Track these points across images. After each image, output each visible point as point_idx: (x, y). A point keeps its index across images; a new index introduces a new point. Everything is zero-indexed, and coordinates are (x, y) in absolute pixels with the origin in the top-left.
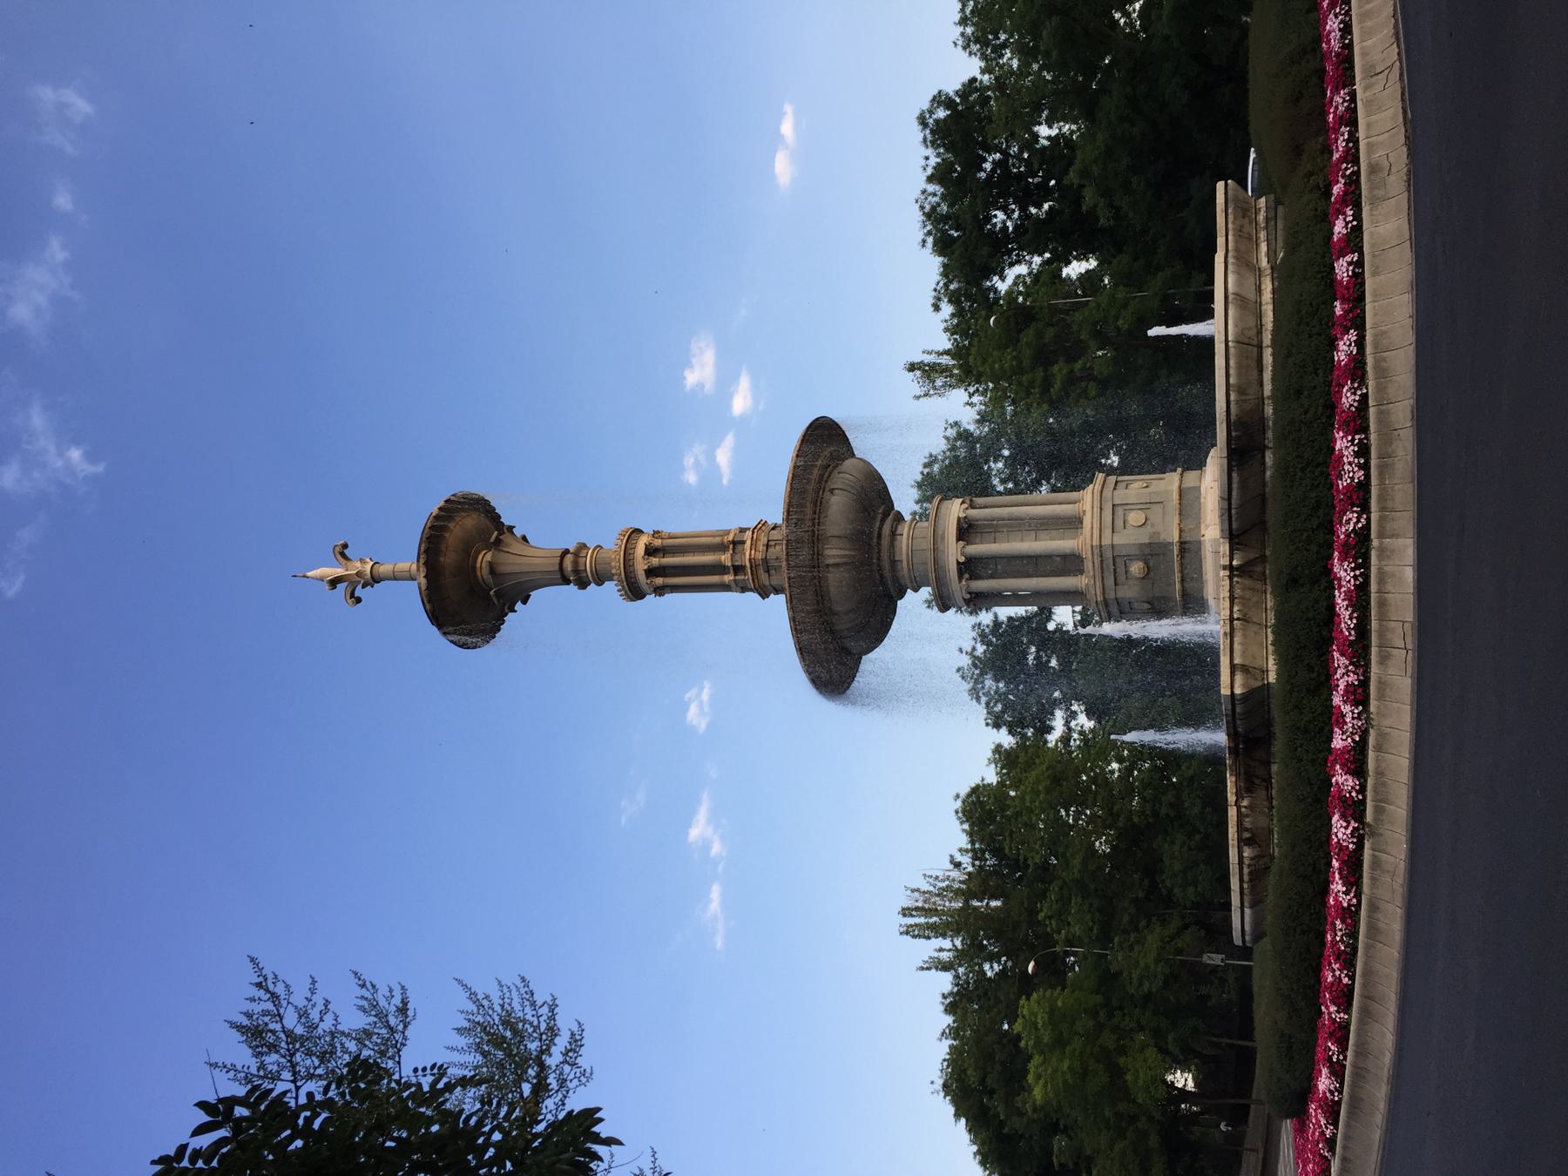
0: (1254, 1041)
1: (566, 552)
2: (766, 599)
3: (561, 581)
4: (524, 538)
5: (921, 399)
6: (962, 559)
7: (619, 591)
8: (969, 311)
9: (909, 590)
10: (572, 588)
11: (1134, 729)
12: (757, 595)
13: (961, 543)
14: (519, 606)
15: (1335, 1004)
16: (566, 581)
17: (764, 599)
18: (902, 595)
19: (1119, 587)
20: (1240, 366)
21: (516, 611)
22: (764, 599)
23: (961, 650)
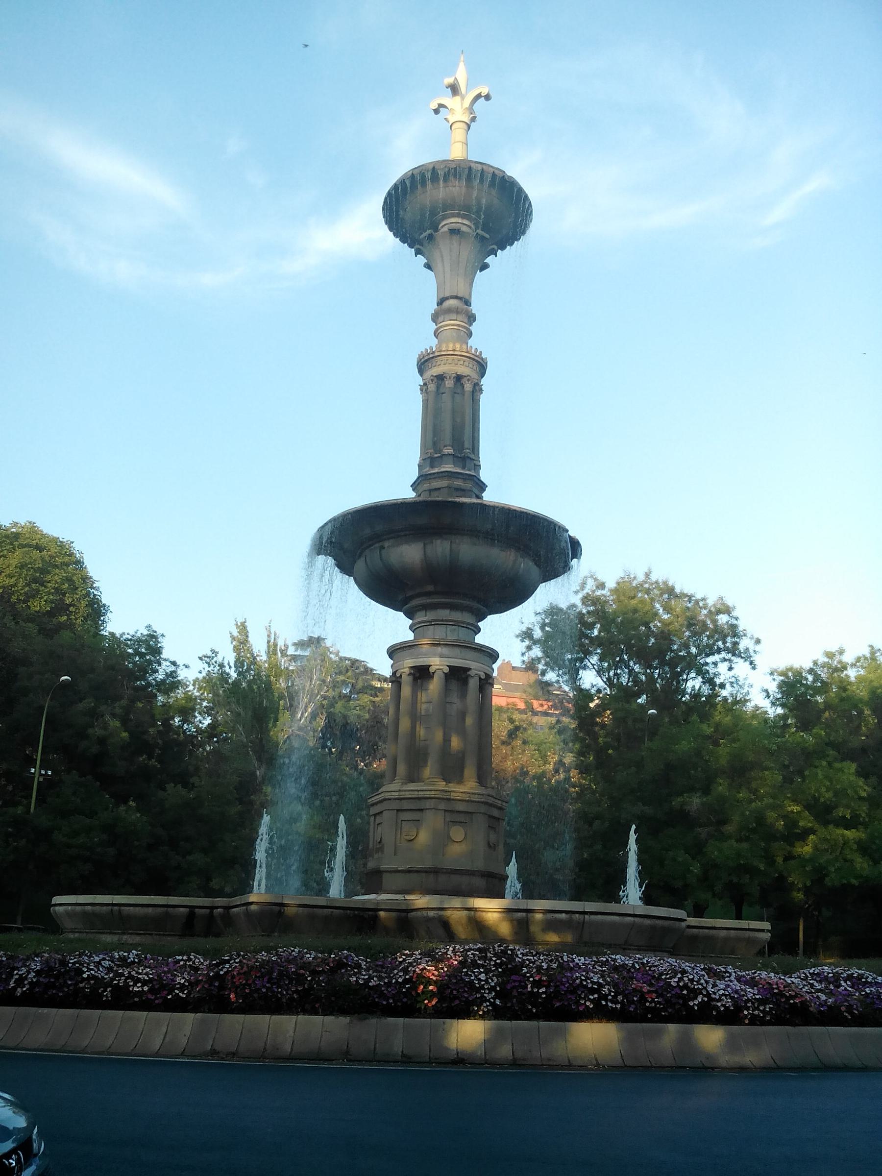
0: (769, 956)
1: (468, 303)
2: (411, 488)
3: (442, 296)
4: (485, 267)
5: (172, 659)
6: (432, 670)
7: (431, 348)
8: (796, 696)
9: (411, 621)
10: (433, 306)
11: (345, 817)
12: (416, 478)
13: (446, 670)
14: (421, 260)
15: (55, 993)
16: (441, 302)
17: (411, 486)
18: (409, 614)
19: (443, 812)
20: (613, 924)
21: (416, 256)
22: (411, 486)
23: (187, 667)
